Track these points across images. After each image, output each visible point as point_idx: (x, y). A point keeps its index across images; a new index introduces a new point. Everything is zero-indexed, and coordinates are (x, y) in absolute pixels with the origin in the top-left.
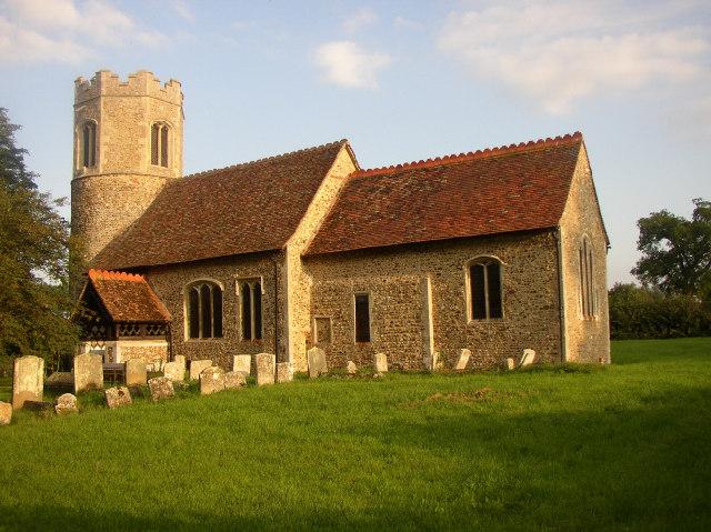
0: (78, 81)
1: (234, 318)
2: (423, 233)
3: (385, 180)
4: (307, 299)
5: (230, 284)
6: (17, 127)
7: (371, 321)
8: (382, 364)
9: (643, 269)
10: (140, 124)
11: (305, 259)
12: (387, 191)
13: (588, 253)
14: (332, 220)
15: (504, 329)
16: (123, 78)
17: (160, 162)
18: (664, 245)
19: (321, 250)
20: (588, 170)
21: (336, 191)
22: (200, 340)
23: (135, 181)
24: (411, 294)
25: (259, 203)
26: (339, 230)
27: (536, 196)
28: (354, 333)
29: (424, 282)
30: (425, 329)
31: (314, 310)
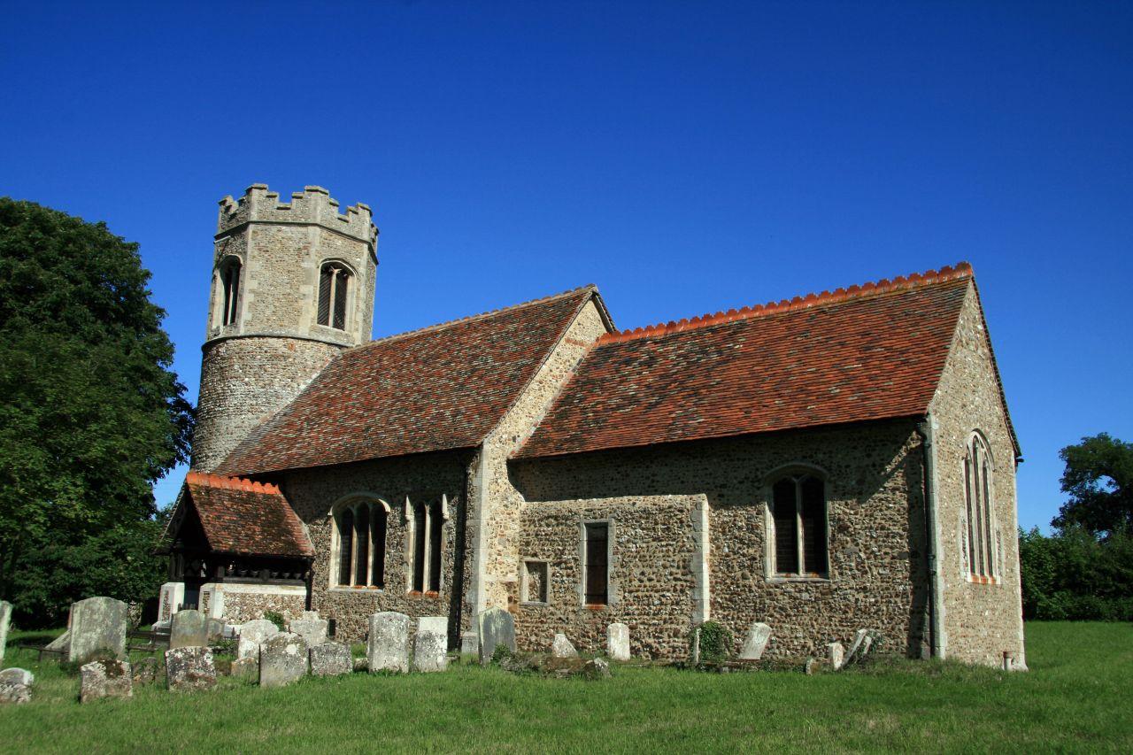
3: (649, 346)
4: (514, 529)
6: (147, 275)
7: (611, 569)
8: (619, 643)
9: (1068, 517)
10: (304, 265)
11: (519, 469)
12: (649, 363)
13: (980, 466)
14: (564, 406)
15: (832, 592)
18: (1104, 484)
19: (540, 452)
20: (980, 327)
21: (574, 363)
23: (291, 347)
24: (672, 528)
25: (455, 379)
26: (572, 423)
27: (888, 366)
28: (583, 588)
29: (698, 506)
30: (695, 586)
31: (524, 547)
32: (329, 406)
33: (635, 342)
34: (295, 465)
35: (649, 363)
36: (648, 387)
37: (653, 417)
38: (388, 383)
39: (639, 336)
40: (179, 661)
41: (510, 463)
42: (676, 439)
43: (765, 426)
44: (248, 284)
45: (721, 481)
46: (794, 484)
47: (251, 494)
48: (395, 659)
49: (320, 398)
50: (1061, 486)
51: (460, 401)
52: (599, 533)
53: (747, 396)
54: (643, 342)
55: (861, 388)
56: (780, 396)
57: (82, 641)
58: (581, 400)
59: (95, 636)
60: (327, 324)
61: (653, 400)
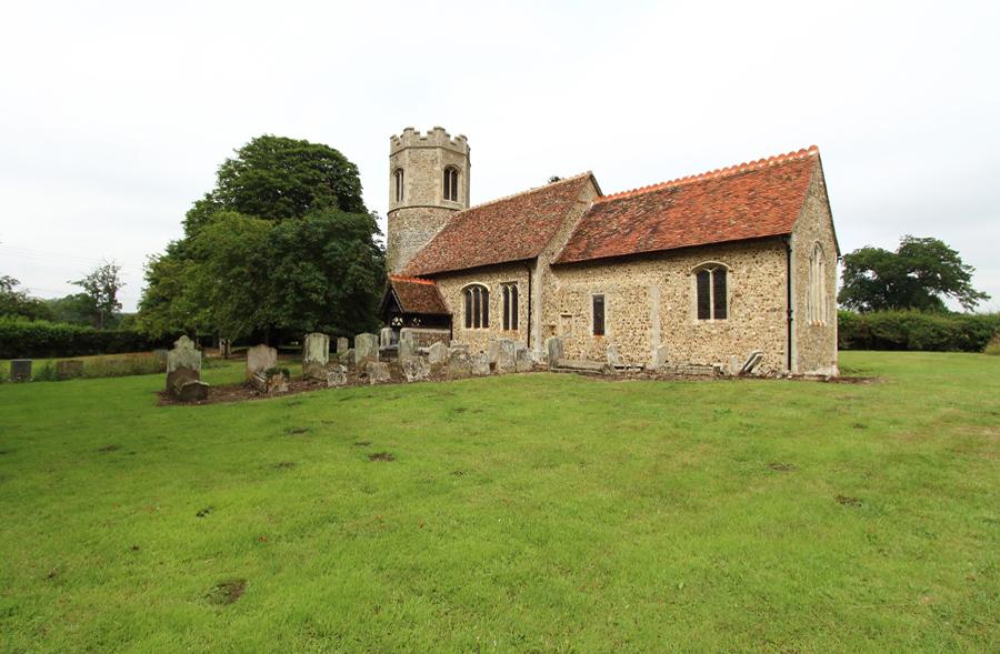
0: (392, 138)
1: (496, 314)
2: (655, 244)
5: (493, 285)
16: (424, 134)
17: (496, 314)
22: (472, 329)
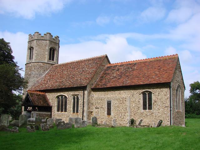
7: (112, 109)
12: (118, 70)
18: (198, 91)
26: (103, 81)
28: (106, 113)
32: (53, 76)
33: (114, 66)
34: (47, 88)
35: (118, 70)
36: (118, 75)
37: (120, 81)
38: (65, 72)
39: (115, 65)
40: (43, 126)
41: (143, 109)
42: (124, 85)
43: (142, 83)
44: (35, 52)
45: (133, 93)
46: (146, 94)
47: (40, 94)
48: (79, 125)
49: (51, 75)
50: (189, 92)
51: (81, 76)
52: (109, 103)
53: (138, 77)
54: (116, 66)
55: (159, 77)
56: (144, 77)
57: (21, 122)
58: (105, 77)
59: (23, 121)
60: (51, 60)
61: (120, 77)
